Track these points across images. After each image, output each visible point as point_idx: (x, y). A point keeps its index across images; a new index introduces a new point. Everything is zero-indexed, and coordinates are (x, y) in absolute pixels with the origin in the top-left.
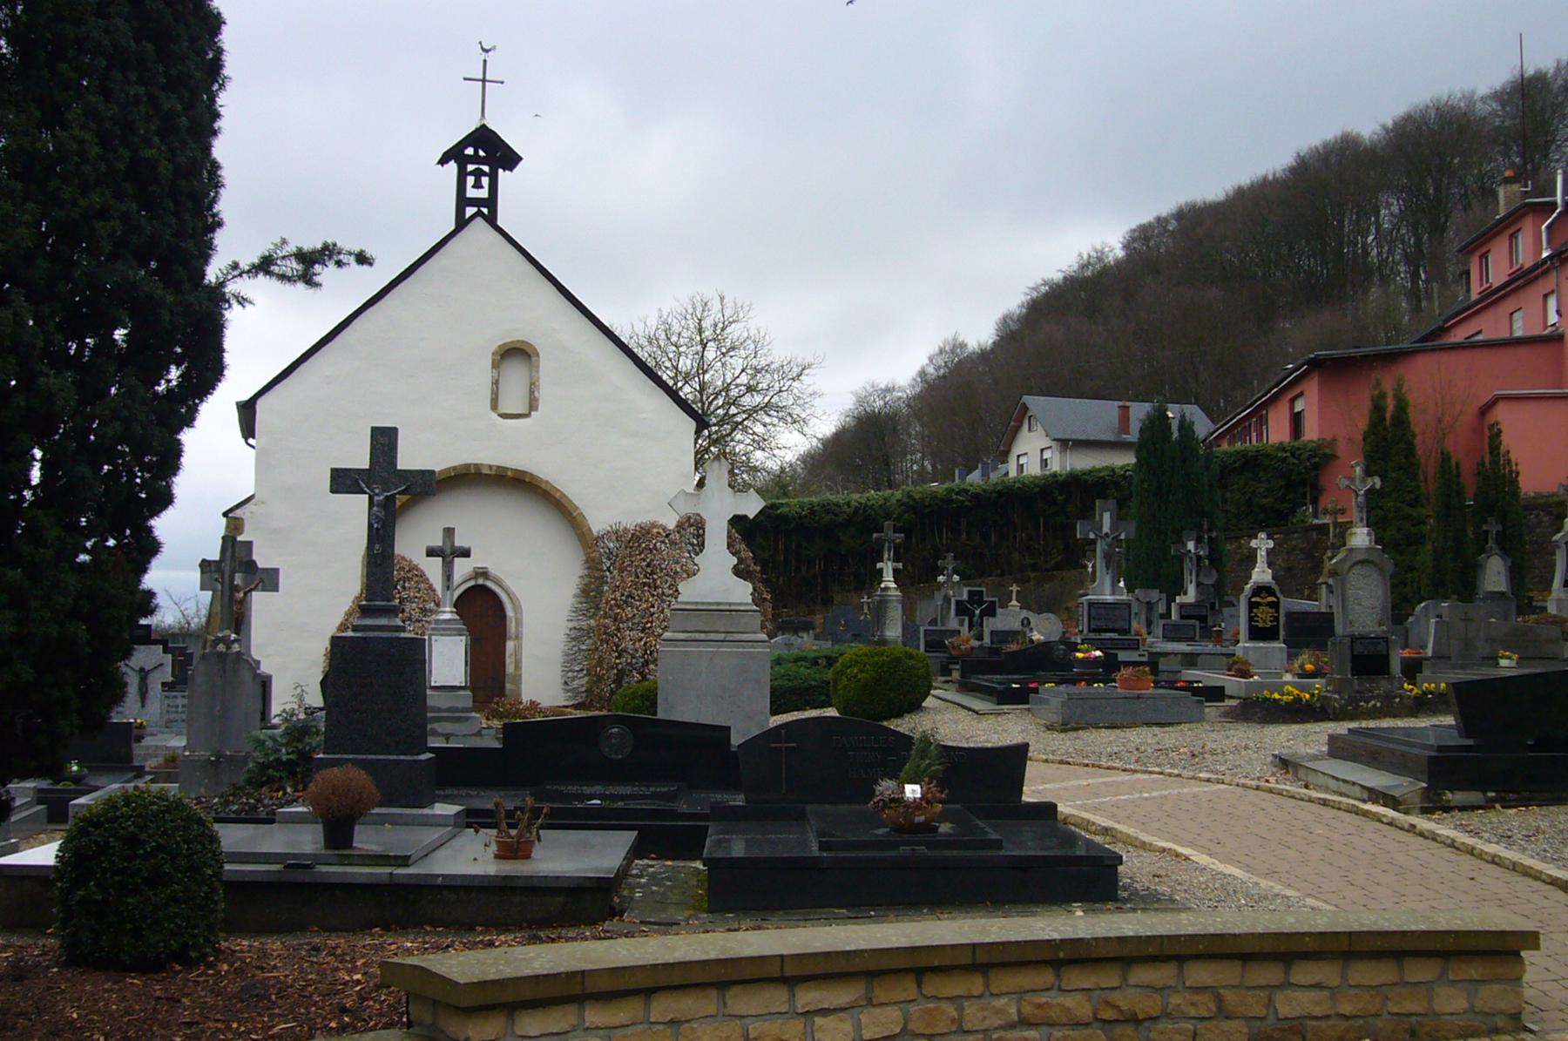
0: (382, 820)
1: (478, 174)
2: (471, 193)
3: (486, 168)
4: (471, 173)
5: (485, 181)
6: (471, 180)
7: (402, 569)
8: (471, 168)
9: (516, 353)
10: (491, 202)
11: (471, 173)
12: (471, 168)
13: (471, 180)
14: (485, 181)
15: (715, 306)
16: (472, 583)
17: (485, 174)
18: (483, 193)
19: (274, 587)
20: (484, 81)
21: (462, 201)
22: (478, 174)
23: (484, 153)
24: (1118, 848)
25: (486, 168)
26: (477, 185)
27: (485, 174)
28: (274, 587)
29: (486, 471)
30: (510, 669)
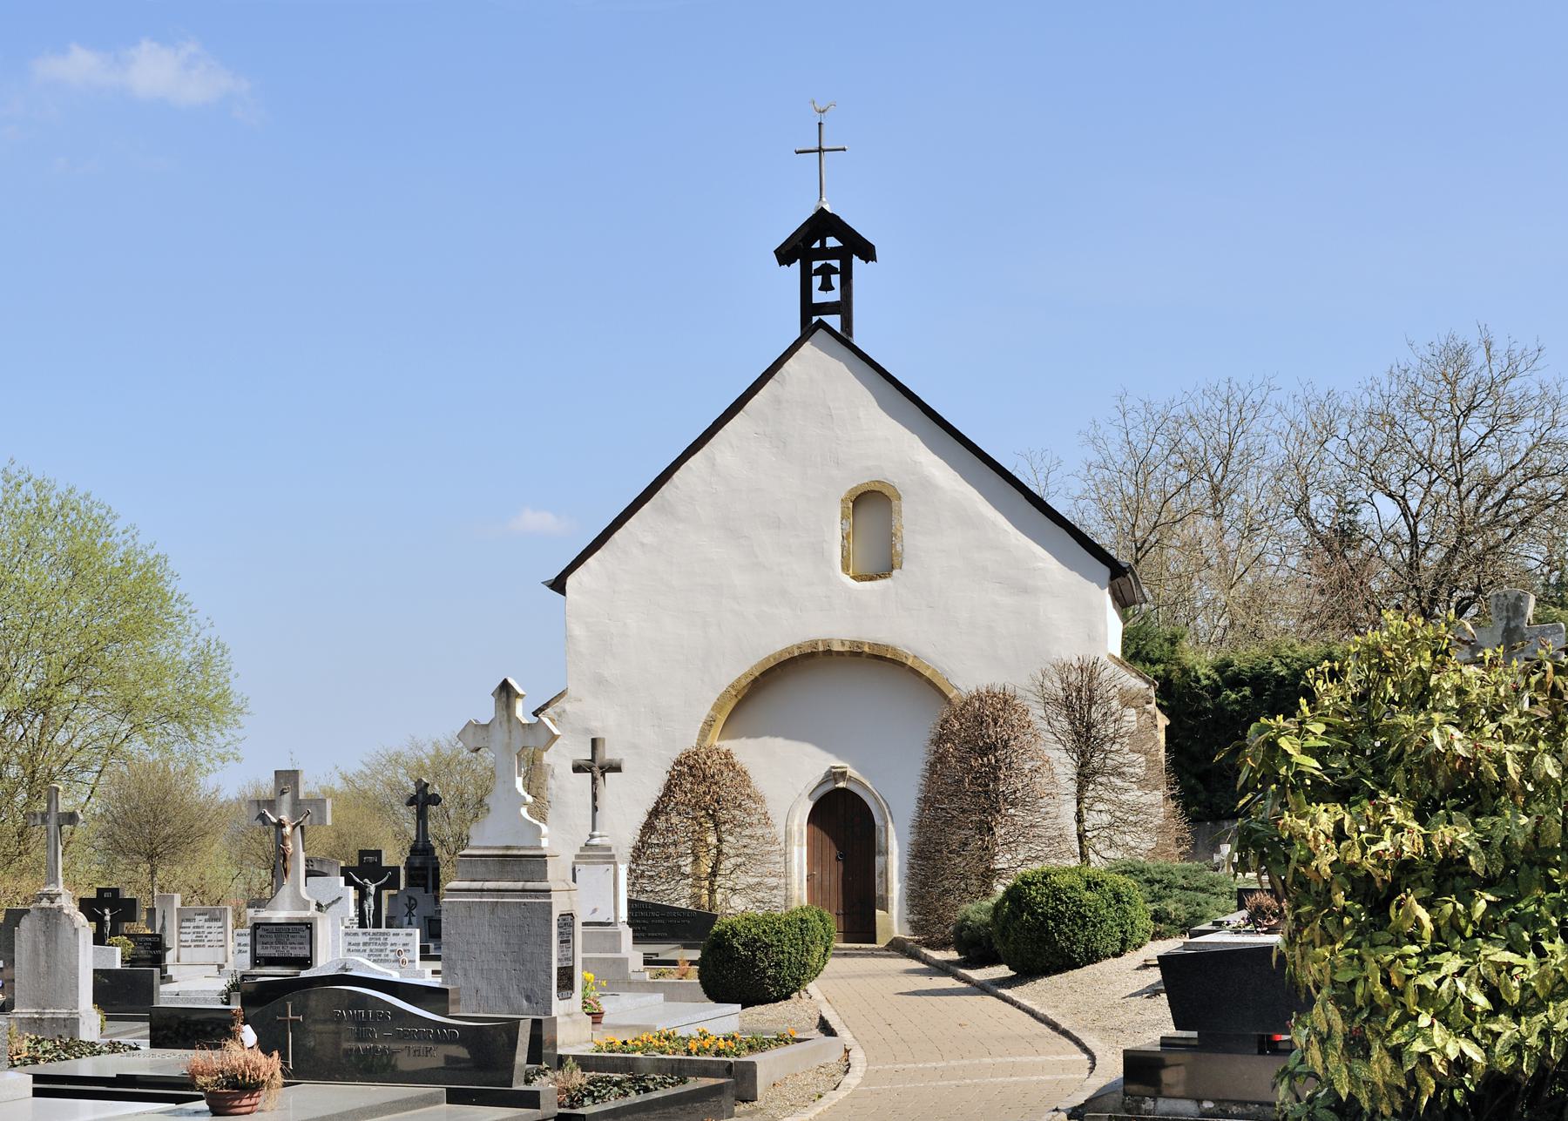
0: (163, 928)
1: (826, 272)
2: (818, 297)
3: (836, 263)
4: (818, 272)
5: (836, 280)
6: (817, 281)
7: (460, 764)
8: (816, 265)
9: (871, 503)
10: (843, 308)
11: (818, 272)
12: (816, 265)
13: (817, 281)
14: (836, 280)
15: (1479, 358)
16: (829, 787)
17: (834, 271)
18: (834, 296)
19: (294, 775)
20: (820, 150)
21: (809, 309)
22: (826, 272)
23: (824, 248)
24: (746, 1058)
25: (836, 263)
26: (826, 286)
27: (834, 271)
28: (294, 775)
29: (836, 647)
30: (879, 892)
